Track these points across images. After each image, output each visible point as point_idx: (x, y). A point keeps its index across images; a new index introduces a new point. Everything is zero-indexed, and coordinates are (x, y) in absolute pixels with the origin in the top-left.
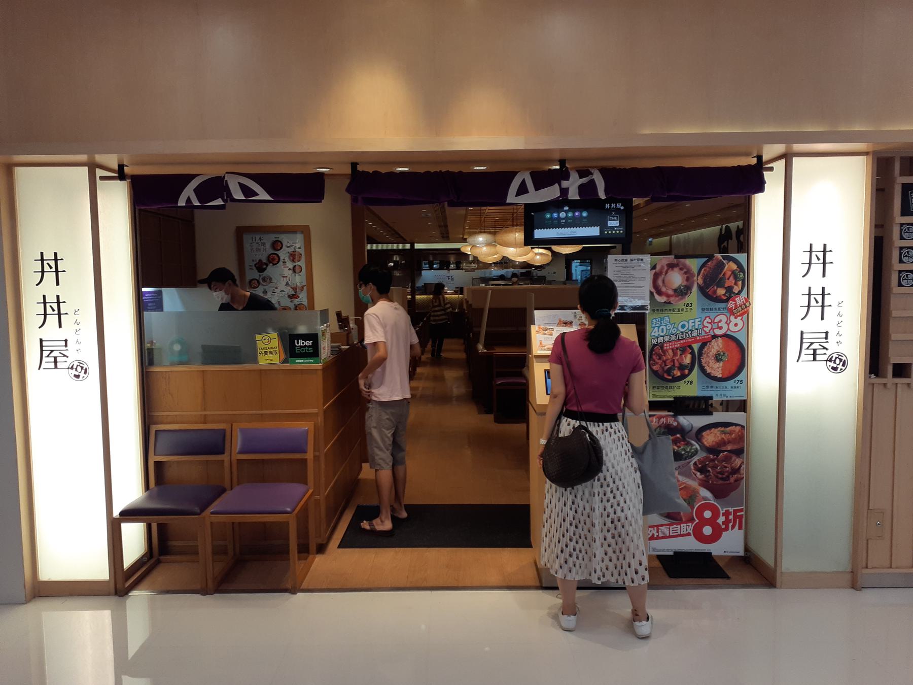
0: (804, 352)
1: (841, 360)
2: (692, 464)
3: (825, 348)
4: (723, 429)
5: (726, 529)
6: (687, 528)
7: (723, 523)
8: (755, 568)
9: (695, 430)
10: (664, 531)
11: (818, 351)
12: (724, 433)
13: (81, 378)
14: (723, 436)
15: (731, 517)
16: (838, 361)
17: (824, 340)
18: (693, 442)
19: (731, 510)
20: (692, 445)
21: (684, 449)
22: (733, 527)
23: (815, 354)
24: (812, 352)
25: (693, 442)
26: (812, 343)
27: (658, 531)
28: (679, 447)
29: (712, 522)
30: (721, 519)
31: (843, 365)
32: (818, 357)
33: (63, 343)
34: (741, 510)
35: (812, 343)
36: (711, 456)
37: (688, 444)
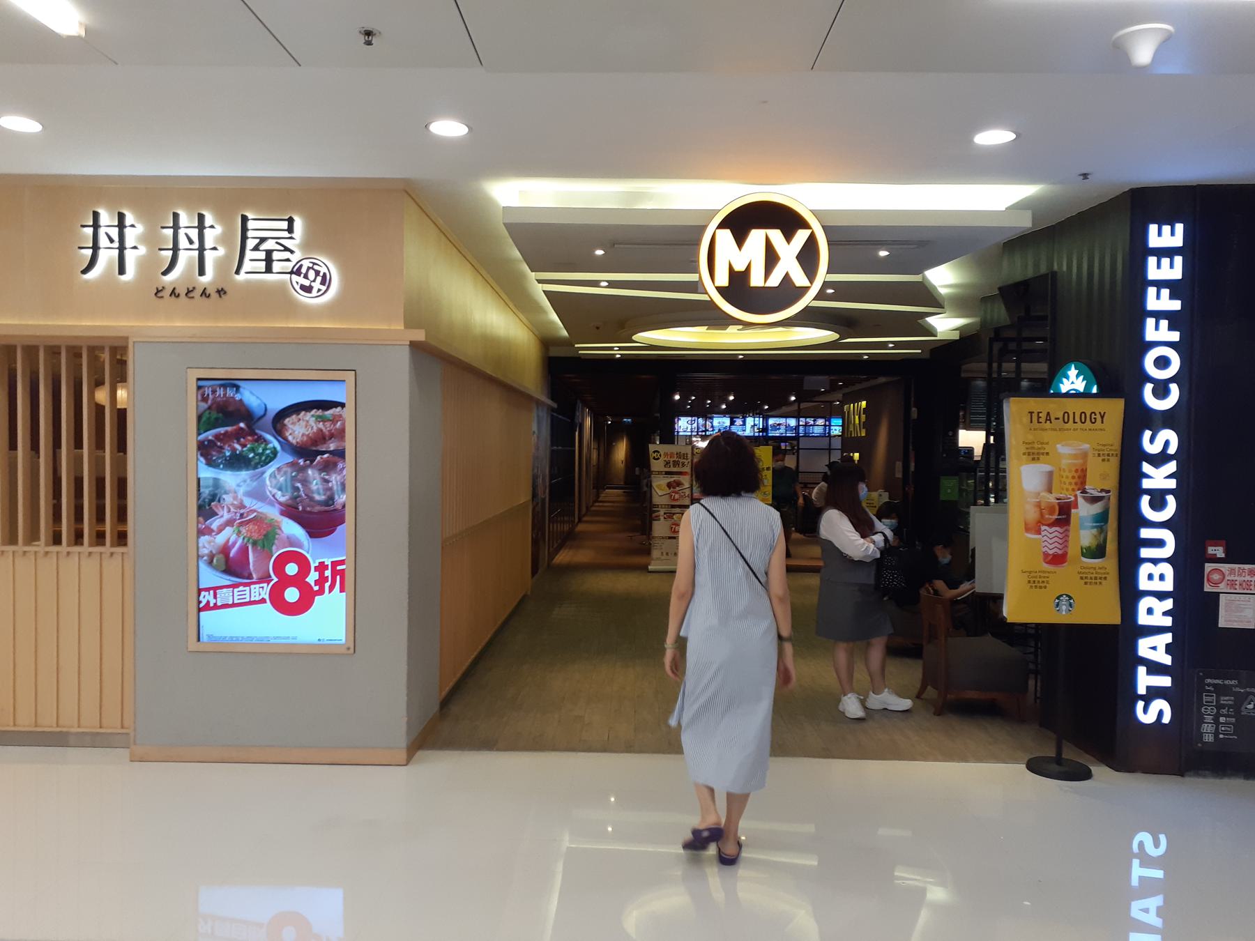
0: (249, 254)
1: (317, 273)
2: (267, 475)
3: (286, 249)
4: (320, 412)
5: (321, 592)
6: (263, 591)
7: (316, 582)
8: (445, 703)
9: (271, 415)
10: (225, 596)
11: (276, 256)
12: (321, 419)
13: (314, 293)
14: (321, 425)
15: (328, 573)
16: (312, 274)
17: (286, 234)
18: (269, 437)
19: (328, 562)
20: (266, 442)
21: (252, 450)
22: (331, 588)
23: (269, 260)
24: (262, 255)
25: (269, 437)
26: (263, 240)
27: (215, 597)
28: (244, 446)
29: (298, 581)
30: (313, 577)
31: (323, 283)
32: (276, 266)
33: (285, 225)
34: (342, 562)
35: (263, 240)
36: (301, 462)
37: (260, 440)
